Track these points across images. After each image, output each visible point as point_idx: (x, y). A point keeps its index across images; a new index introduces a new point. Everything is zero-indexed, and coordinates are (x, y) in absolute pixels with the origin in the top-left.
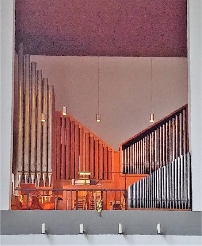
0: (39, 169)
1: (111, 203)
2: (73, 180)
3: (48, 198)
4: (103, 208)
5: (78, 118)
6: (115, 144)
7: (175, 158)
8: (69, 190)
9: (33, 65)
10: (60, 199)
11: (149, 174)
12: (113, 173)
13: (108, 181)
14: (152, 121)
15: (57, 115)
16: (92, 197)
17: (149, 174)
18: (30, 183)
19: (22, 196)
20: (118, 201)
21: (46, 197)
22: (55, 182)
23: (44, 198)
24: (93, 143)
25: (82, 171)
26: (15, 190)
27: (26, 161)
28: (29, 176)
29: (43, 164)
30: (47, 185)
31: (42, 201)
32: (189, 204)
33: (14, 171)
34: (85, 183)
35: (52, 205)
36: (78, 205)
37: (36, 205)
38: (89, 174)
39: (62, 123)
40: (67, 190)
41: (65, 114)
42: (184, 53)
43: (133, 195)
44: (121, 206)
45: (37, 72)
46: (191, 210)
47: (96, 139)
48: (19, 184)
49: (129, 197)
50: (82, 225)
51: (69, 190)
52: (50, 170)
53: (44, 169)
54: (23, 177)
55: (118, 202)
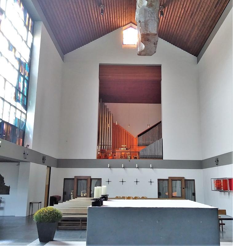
0: (107, 144)
7: (160, 138)
9: (105, 106)
14: (148, 127)
15: (114, 125)
20: (136, 156)
28: (104, 147)
33: (98, 145)
35: (112, 157)
36: (121, 157)
42: (157, 99)
45: (107, 109)
53: (109, 144)
55: (136, 156)
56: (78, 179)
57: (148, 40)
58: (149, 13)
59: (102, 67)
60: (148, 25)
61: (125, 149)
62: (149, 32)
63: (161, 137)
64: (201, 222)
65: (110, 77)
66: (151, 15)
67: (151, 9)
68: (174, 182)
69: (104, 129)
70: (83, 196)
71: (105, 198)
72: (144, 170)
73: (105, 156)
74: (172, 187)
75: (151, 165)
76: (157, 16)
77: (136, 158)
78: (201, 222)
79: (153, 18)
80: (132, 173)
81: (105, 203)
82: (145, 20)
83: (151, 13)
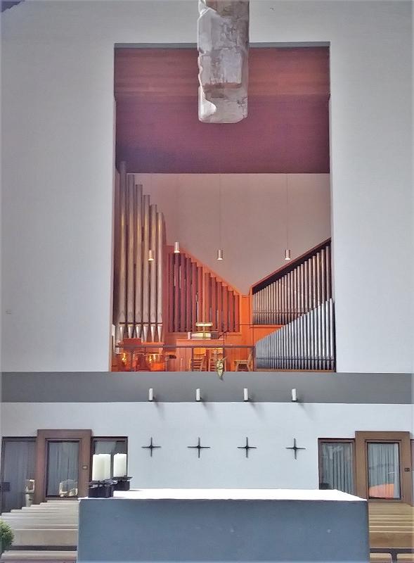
0: (146, 320)
1: (235, 362)
2: (189, 333)
3: (157, 356)
4: (228, 368)
5: (196, 254)
6: (242, 286)
7: (326, 300)
8: (183, 347)
9: (138, 188)
10: (172, 357)
11: (305, 313)
12: (241, 326)
13: (234, 333)
14: (287, 259)
15: (167, 250)
16: (213, 354)
17: (288, 323)
18: (134, 338)
19: (124, 354)
20: (243, 359)
21: (154, 355)
22: (166, 336)
23: (152, 356)
24: (215, 285)
25: (201, 321)
26: (116, 347)
27: (130, 309)
28: (134, 329)
29: (151, 314)
30: (156, 340)
31: (150, 360)
32: (332, 364)
33: (115, 320)
34: (204, 337)
35: (164, 365)
36: (195, 366)
37: (143, 366)
38: (210, 325)
39: (178, 263)
40: (180, 347)
41: (178, 252)
42: (323, 166)
43: (262, 351)
44: (248, 366)
45: (143, 197)
46: (335, 372)
47: (218, 280)
48: (122, 339)
49: (258, 355)
50: (198, 391)
51: (183, 347)
52: (160, 320)
53: (153, 320)
54: (126, 330)
55: (243, 362)
56: (50, 439)
57: (222, 96)
58: (223, 32)
59: (122, 53)
60: (219, 61)
61: (209, 335)
62: (223, 79)
63: (331, 297)
64: (329, 531)
65: (151, 89)
66: (227, 35)
67: (227, 20)
68: (374, 448)
69: (135, 266)
70: (66, 497)
71: (123, 484)
72: (271, 408)
73: (139, 362)
74: (368, 468)
75: (294, 391)
76: (242, 38)
77: (243, 367)
78: (329, 531)
79: (233, 44)
80: (233, 418)
81: (118, 494)
82: (213, 48)
83: (229, 30)
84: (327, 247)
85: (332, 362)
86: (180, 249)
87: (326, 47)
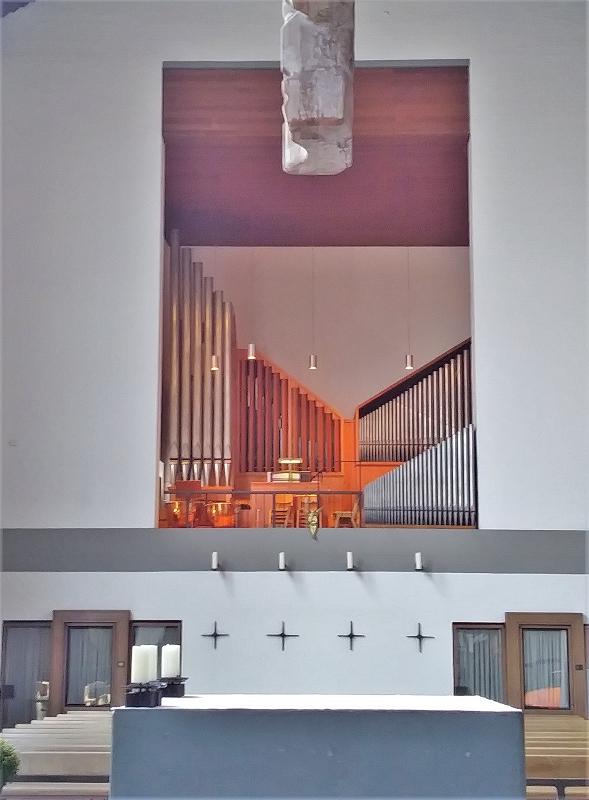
0: (207, 454)
1: (335, 515)
2: (269, 473)
3: (223, 506)
4: (324, 522)
5: (279, 361)
6: (344, 406)
7: (463, 426)
8: (260, 493)
9: (196, 267)
10: (244, 507)
11: (434, 445)
12: (342, 463)
13: (333, 473)
14: (409, 368)
15: (238, 355)
16: (303, 504)
17: (409, 459)
18: (191, 480)
19: (177, 503)
20: (345, 511)
21: (219, 504)
22: (236, 477)
23: (217, 506)
24: (306, 405)
25: (287, 457)
26: (165, 492)
27: (185, 440)
28: (191, 467)
29: (215, 446)
30: (222, 483)
31: (214, 511)
32: (473, 518)
33: (163, 455)
34: (290, 479)
35: (233, 518)
36: (277, 520)
37: (203, 520)
38: (298, 462)
39: (253, 374)
40: (256, 493)
41: (254, 358)
42: (459, 236)
43: (373, 498)
44: (352, 520)
45: (204, 281)
46: (477, 528)
47: (310, 398)
48: (173, 482)
49: (366, 504)
50: (282, 555)
51: (260, 493)
52: (227, 455)
53: (218, 455)
54: (179, 469)
55: (346, 514)
56: (72, 624)
57: (315, 137)
58: (317, 45)
59: (173, 75)
60: (312, 86)
61: (297, 476)
62: (318, 112)
63: (470, 422)
64: (468, 754)
65: (215, 127)
66: (323, 50)
67: (323, 28)
68: (532, 637)
69: (192, 378)
70: (94, 706)
71: (175, 687)
72: (386, 580)
73: (198, 514)
74: (523, 666)
75: (418, 556)
76: (344, 54)
77: (345, 522)
78: (468, 754)
79: (331, 63)
80: (332, 594)
81: (167, 702)
82: (303, 68)
83: (325, 42)
84: (465, 352)
85: (473, 514)
86: (256, 354)
87: (463, 67)
